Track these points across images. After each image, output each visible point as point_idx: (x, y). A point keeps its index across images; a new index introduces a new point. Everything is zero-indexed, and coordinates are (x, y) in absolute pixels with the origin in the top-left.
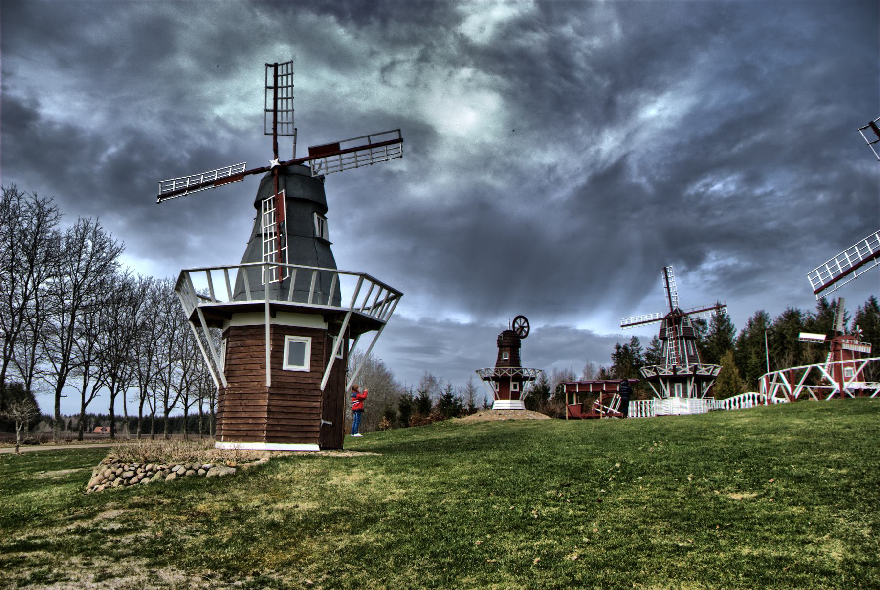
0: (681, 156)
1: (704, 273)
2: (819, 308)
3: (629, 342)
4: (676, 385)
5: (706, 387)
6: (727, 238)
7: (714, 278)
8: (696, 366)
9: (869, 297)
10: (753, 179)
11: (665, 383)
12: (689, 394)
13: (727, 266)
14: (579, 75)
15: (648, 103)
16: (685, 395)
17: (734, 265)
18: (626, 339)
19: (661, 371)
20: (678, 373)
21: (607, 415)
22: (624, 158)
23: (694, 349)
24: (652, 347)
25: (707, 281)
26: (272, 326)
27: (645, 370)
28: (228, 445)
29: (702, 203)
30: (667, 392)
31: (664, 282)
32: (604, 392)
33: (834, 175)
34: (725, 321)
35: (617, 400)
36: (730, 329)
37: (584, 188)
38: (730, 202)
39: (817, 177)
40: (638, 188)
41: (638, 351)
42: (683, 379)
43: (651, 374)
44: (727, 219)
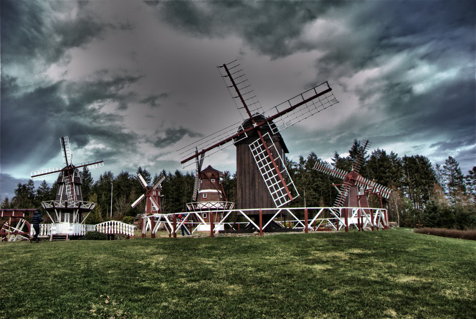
1: (86, 150)
3: (27, 183)
4: (65, 214)
5: (86, 216)
6: (100, 134)
7: (91, 154)
8: (81, 203)
9: (162, 170)
10: (123, 107)
11: (58, 212)
12: (74, 220)
13: (99, 148)
14: (43, 29)
16: (71, 221)
17: (103, 149)
18: (25, 180)
19: (56, 204)
20: (68, 207)
21: (13, 233)
22: (60, 83)
23: (80, 192)
24: (42, 187)
25: (86, 155)
27: (45, 204)
29: (95, 114)
30: (59, 219)
31: (63, 153)
32: (12, 217)
34: (88, 176)
35: (22, 223)
36: (90, 180)
37: (31, 94)
38: (110, 117)
40: (60, 100)
41: (32, 189)
42: (71, 211)
43: (48, 206)
44: (104, 124)
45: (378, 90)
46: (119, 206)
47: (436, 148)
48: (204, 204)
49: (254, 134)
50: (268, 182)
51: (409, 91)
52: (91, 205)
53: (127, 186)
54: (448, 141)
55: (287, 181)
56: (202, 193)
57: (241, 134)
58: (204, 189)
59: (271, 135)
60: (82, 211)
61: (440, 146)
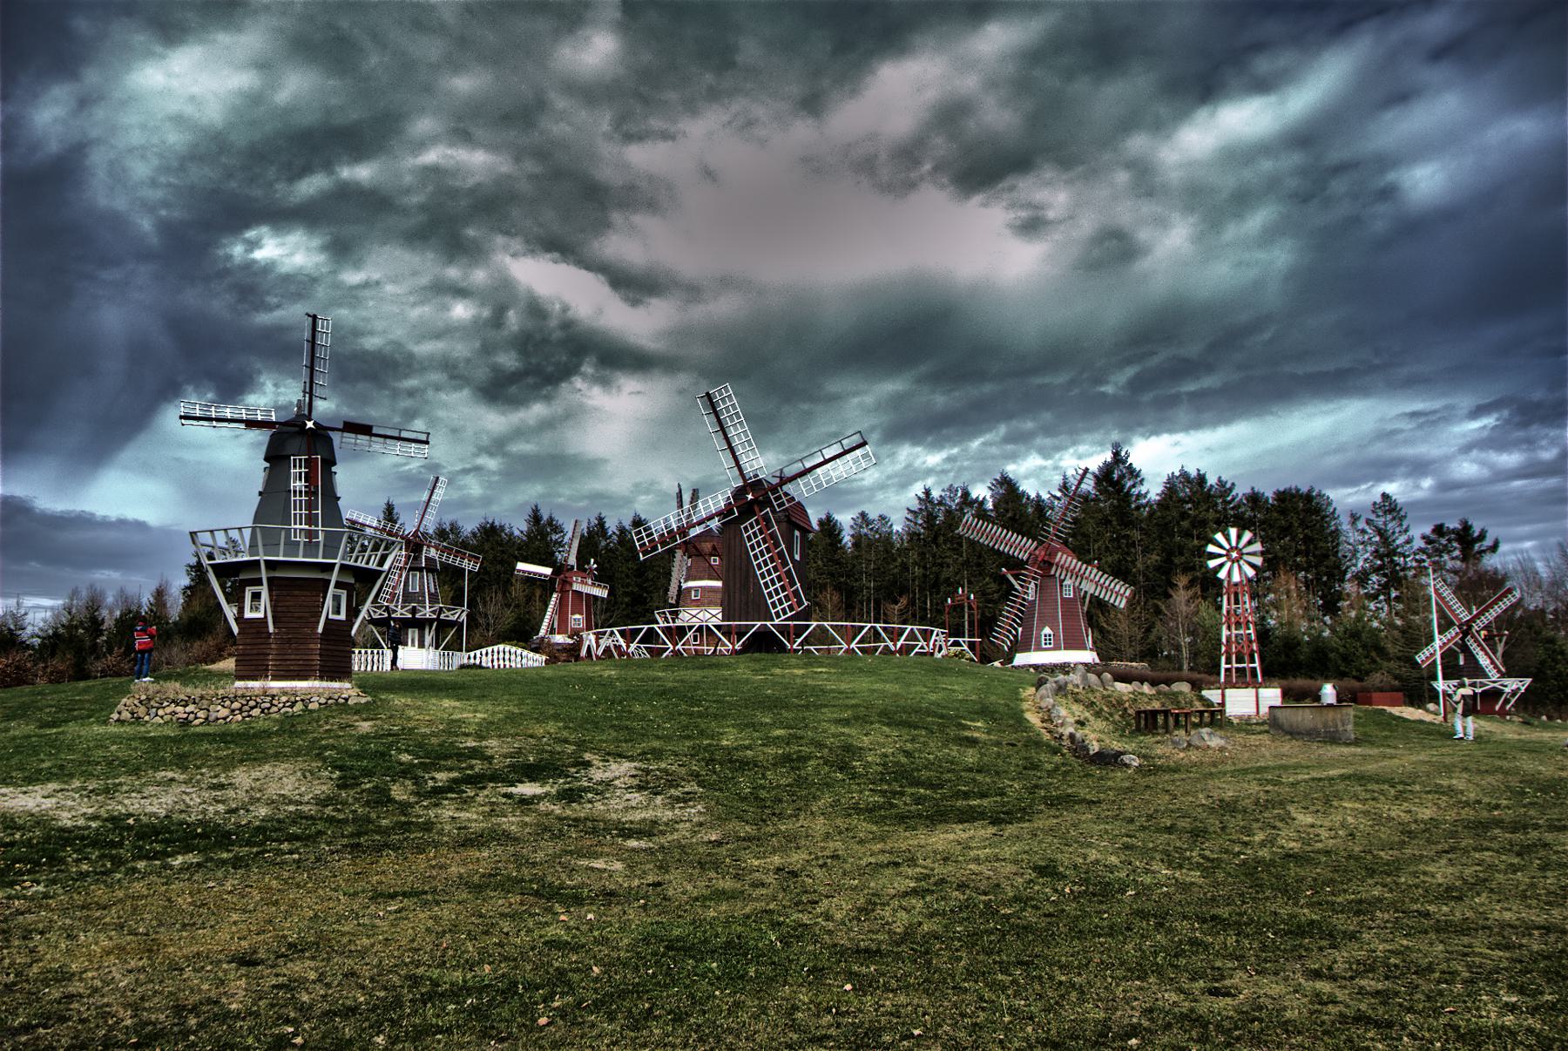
0: (200, 174)
2: (528, 522)
10: (342, 251)
15: (148, 54)
26: (269, 579)
28: (276, 685)
33: (479, 276)
38: (297, 285)
39: (453, 273)
42: (421, 625)
45: (1271, 186)
46: (486, 616)
47: (1489, 421)
48: (694, 612)
49: (747, 510)
50: (766, 584)
51: (1389, 193)
52: (460, 615)
53: (501, 562)
54: (1538, 395)
55: (792, 583)
56: (689, 589)
57: (728, 510)
58: (695, 579)
59: (774, 511)
60: (443, 626)
61: (1506, 413)
